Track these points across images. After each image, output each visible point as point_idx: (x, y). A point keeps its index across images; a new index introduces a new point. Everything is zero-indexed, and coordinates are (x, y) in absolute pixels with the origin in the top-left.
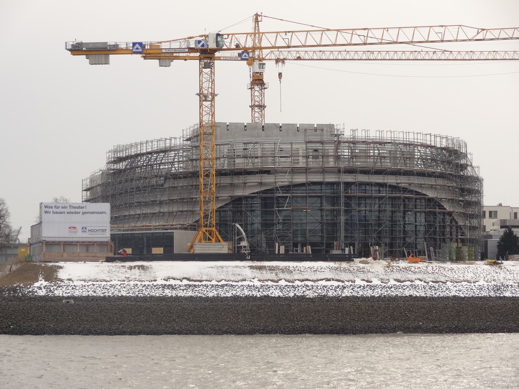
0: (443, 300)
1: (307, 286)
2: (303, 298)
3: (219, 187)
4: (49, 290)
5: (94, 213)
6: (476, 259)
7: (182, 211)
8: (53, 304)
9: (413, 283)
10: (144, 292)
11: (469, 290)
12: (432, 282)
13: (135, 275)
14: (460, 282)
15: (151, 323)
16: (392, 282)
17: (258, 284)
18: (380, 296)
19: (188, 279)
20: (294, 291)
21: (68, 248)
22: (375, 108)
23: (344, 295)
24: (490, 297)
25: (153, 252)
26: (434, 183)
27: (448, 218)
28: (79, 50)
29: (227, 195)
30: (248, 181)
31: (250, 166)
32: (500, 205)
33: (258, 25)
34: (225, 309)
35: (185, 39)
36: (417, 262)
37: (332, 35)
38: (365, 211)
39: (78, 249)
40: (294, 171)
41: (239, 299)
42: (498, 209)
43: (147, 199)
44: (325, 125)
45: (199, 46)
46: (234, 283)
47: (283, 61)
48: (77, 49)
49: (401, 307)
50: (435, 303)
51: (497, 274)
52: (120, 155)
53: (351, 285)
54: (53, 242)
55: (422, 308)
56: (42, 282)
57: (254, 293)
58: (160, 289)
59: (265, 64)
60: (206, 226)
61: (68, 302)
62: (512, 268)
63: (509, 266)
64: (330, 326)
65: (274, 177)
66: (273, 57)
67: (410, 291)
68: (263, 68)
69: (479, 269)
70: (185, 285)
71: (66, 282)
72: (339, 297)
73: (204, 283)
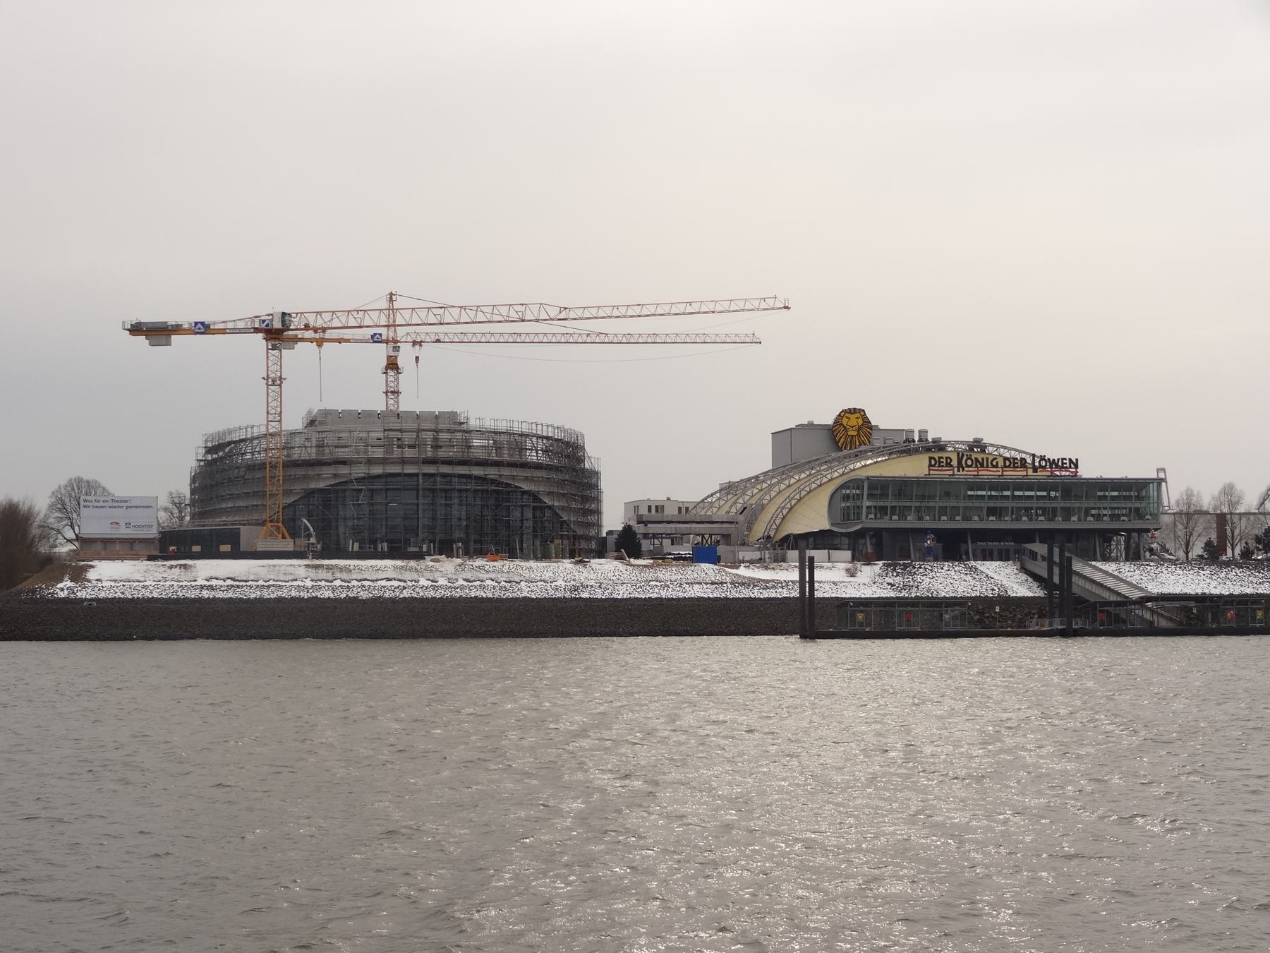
16: (461, 582)
17: (309, 583)
19: (233, 579)
27: (548, 513)
37: (455, 312)
43: (235, 492)
47: (420, 343)
48: (136, 329)
56: (67, 583)
66: (409, 339)
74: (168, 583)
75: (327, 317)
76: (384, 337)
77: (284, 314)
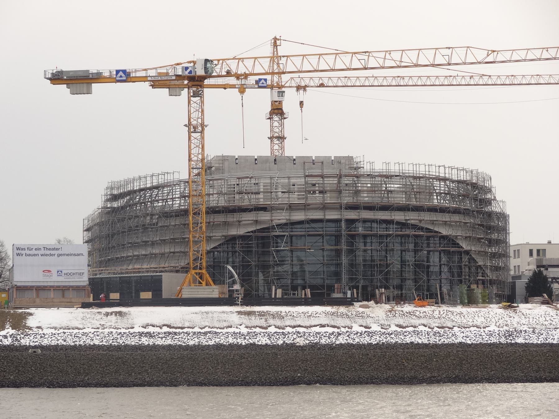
0: (447, 347)
1: (299, 333)
2: (292, 346)
3: (211, 226)
4: (15, 339)
5: (71, 255)
6: (490, 302)
7: (174, 253)
8: (17, 353)
9: (416, 329)
10: (118, 341)
11: (478, 336)
12: (438, 327)
13: (111, 321)
14: (468, 328)
15: (120, 374)
16: (393, 328)
17: (244, 330)
18: (377, 344)
19: (169, 326)
20: (284, 338)
21: (41, 293)
22: (393, 138)
23: (338, 343)
24: (500, 343)
25: (142, 297)
26: (448, 220)
27: (465, 259)
28: (58, 79)
29: (220, 234)
30: (243, 219)
31: (246, 203)
32: (549, 242)
33: (277, 49)
34: (204, 358)
35: (172, 65)
36: (424, 306)
37: (330, 59)
38: (371, 250)
39: (52, 294)
40: (291, 207)
41: (222, 347)
42: (548, 248)
44: (344, 157)
45: (187, 73)
46: (219, 331)
47: (305, 88)
48: (57, 78)
49: (398, 355)
50: (438, 350)
51: (511, 319)
52: (115, 192)
53: (347, 332)
54: (24, 287)
55: (422, 356)
56: (9, 331)
57: (239, 340)
58: (136, 337)
59: (284, 92)
60: (195, 268)
61: (35, 352)
62: (528, 312)
63: (525, 310)
64: (317, 377)
65: (270, 215)
67: (412, 338)
68: (282, 96)
69: (491, 313)
70: (165, 333)
71: (35, 330)
72: (333, 344)
73: (185, 330)
74: (107, 331)
75: (249, 63)
76: (269, 82)
77: (207, 61)
